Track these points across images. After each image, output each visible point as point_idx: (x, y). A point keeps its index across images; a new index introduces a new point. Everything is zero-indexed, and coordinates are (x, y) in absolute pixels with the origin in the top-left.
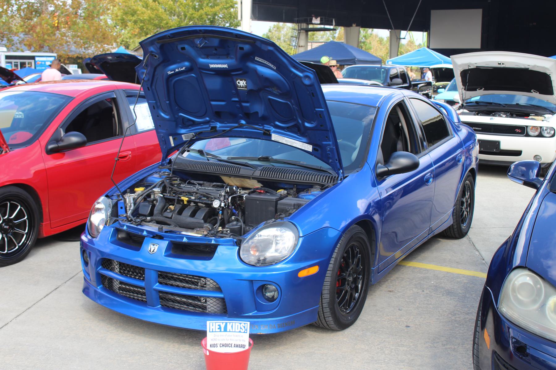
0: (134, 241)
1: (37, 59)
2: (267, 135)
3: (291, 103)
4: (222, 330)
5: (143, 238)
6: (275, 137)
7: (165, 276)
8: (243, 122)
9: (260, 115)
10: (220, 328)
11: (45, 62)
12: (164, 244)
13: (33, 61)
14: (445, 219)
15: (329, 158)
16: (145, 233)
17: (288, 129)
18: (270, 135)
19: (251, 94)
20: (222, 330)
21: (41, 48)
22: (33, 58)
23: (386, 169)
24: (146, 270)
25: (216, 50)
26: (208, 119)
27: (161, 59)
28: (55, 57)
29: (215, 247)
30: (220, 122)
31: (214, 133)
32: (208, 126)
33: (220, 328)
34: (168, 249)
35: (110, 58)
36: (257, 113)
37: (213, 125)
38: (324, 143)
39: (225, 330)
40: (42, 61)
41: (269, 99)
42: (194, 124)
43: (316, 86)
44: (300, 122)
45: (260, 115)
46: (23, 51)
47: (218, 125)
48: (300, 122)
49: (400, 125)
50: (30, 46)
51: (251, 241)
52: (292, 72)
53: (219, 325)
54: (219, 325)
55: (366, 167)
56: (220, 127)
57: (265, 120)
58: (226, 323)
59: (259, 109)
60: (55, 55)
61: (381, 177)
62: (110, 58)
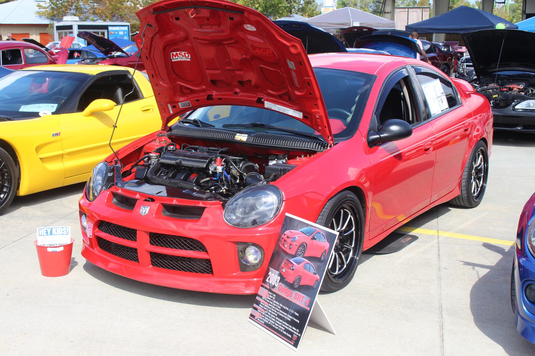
0: (128, 202)
1: (110, 28)
2: (260, 102)
3: (281, 71)
4: (49, 233)
5: (136, 200)
6: (267, 104)
7: (157, 238)
8: (238, 90)
9: (253, 83)
10: (47, 233)
11: (118, 31)
12: (155, 206)
13: (105, 31)
14: (450, 189)
15: (319, 126)
16: (138, 196)
17: (280, 97)
18: (263, 103)
19: (245, 64)
20: (49, 233)
21: (113, 16)
22: (106, 27)
23: (378, 136)
24: (138, 232)
25: (208, 20)
26: (204, 87)
27: (157, 30)
28: (128, 26)
29: (203, 209)
30: (216, 91)
31: (210, 101)
32: (204, 94)
33: (47, 233)
34: (158, 212)
35: (356, 30)
36: (250, 81)
37: (209, 93)
38: (313, 110)
39: (51, 234)
40: (115, 31)
41: (261, 68)
42: (192, 92)
43: (303, 55)
44: (290, 90)
45: (253, 83)
46: (94, 21)
47: (214, 93)
48: (290, 90)
49: (402, 94)
50: (101, 16)
51: (235, 203)
52: (279, 41)
53: (46, 230)
54: (46, 230)
55: (357, 134)
56: (216, 95)
57: (257, 88)
58: (52, 229)
59: (251, 77)
60: (129, 24)
61: (373, 144)
62: (356, 30)
